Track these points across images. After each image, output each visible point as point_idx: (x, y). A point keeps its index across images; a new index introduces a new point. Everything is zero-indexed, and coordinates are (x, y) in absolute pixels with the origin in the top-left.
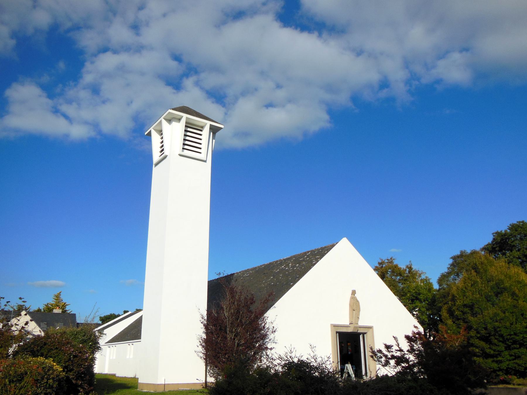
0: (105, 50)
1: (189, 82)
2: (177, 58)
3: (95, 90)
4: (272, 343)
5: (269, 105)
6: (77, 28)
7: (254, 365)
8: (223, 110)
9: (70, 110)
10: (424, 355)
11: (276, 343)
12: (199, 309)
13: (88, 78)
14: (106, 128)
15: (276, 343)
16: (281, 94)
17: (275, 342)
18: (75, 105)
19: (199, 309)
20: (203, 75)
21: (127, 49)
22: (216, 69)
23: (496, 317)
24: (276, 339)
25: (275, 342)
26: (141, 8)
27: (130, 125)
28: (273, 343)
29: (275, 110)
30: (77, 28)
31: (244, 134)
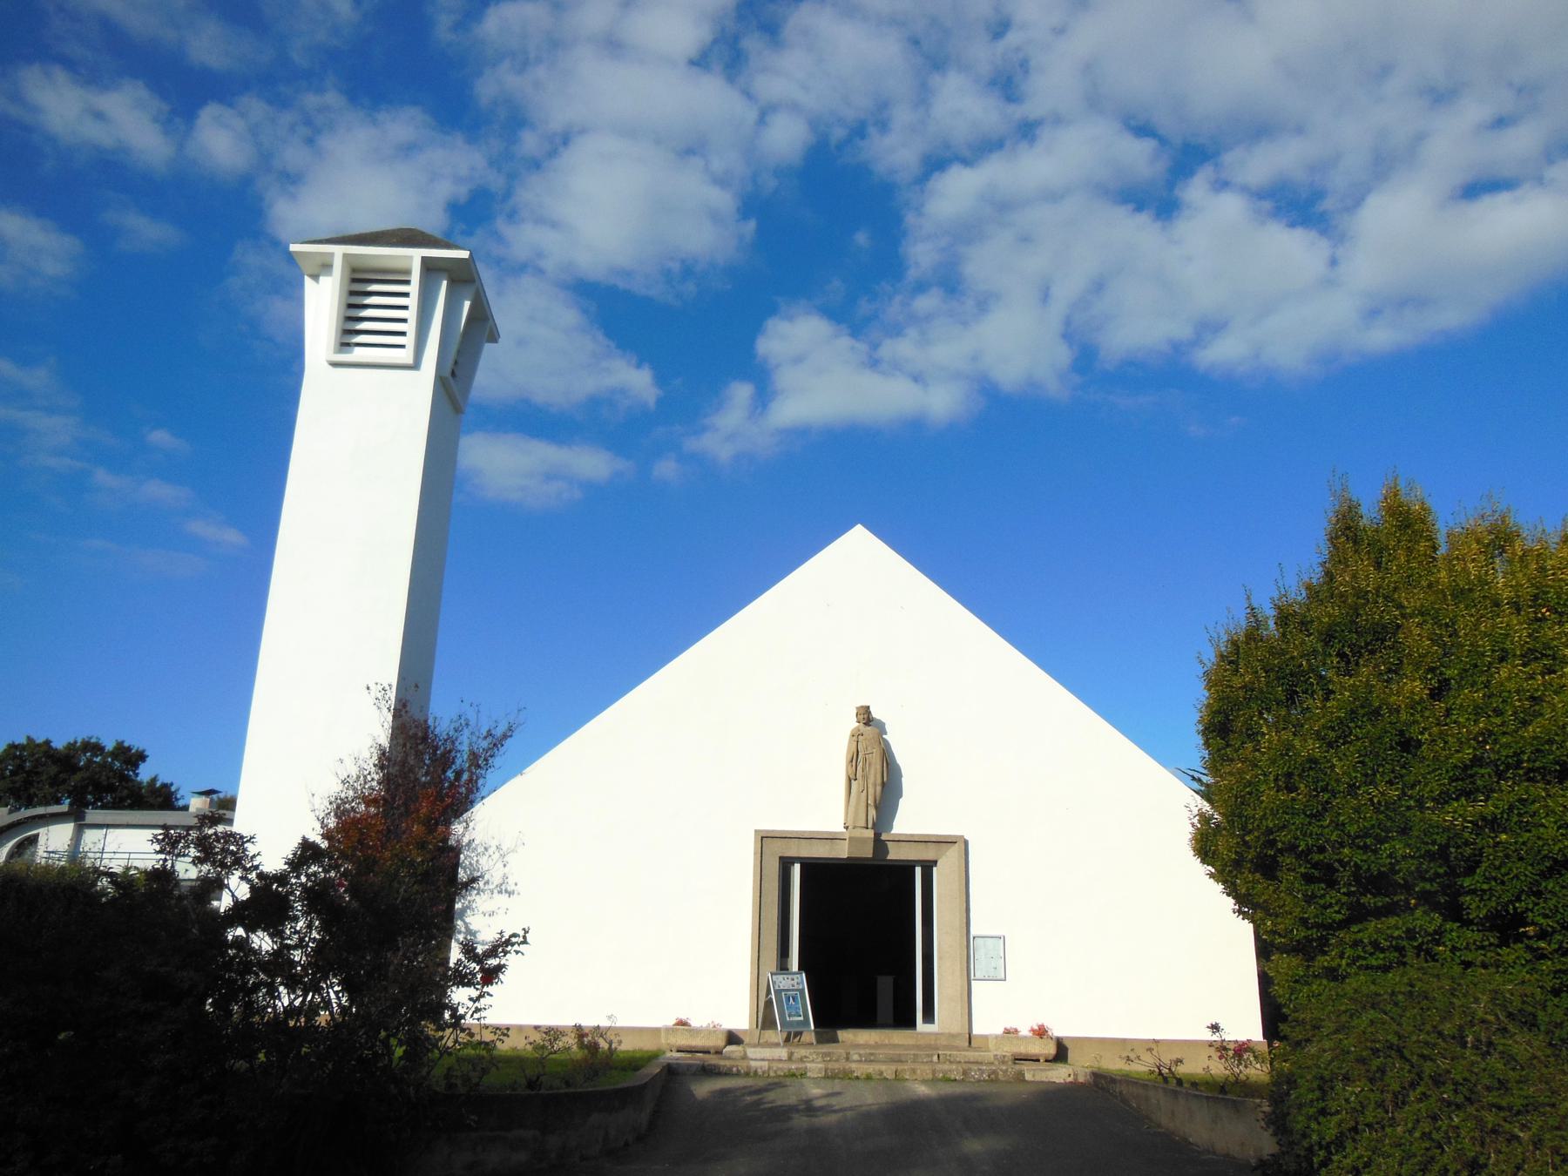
0: (935, 164)
1: (1196, 190)
2: (1142, 130)
3: (949, 282)
4: (495, 891)
5: (1476, 188)
6: (859, 131)
7: (1285, 1069)
8: (1323, 247)
9: (903, 348)
10: (54, 840)
11: (510, 893)
12: (313, 795)
13: (921, 255)
14: (1010, 372)
15: (510, 893)
16: (1522, 141)
17: (506, 891)
18: (912, 333)
19: (313, 795)
20: (1228, 158)
21: (984, 148)
22: (1260, 130)
23: (422, 743)
24: (511, 881)
25: (506, 891)
26: (1000, 28)
27: (1063, 355)
28: (500, 892)
29: (1503, 198)
30: (859, 131)
31: (1407, 301)
